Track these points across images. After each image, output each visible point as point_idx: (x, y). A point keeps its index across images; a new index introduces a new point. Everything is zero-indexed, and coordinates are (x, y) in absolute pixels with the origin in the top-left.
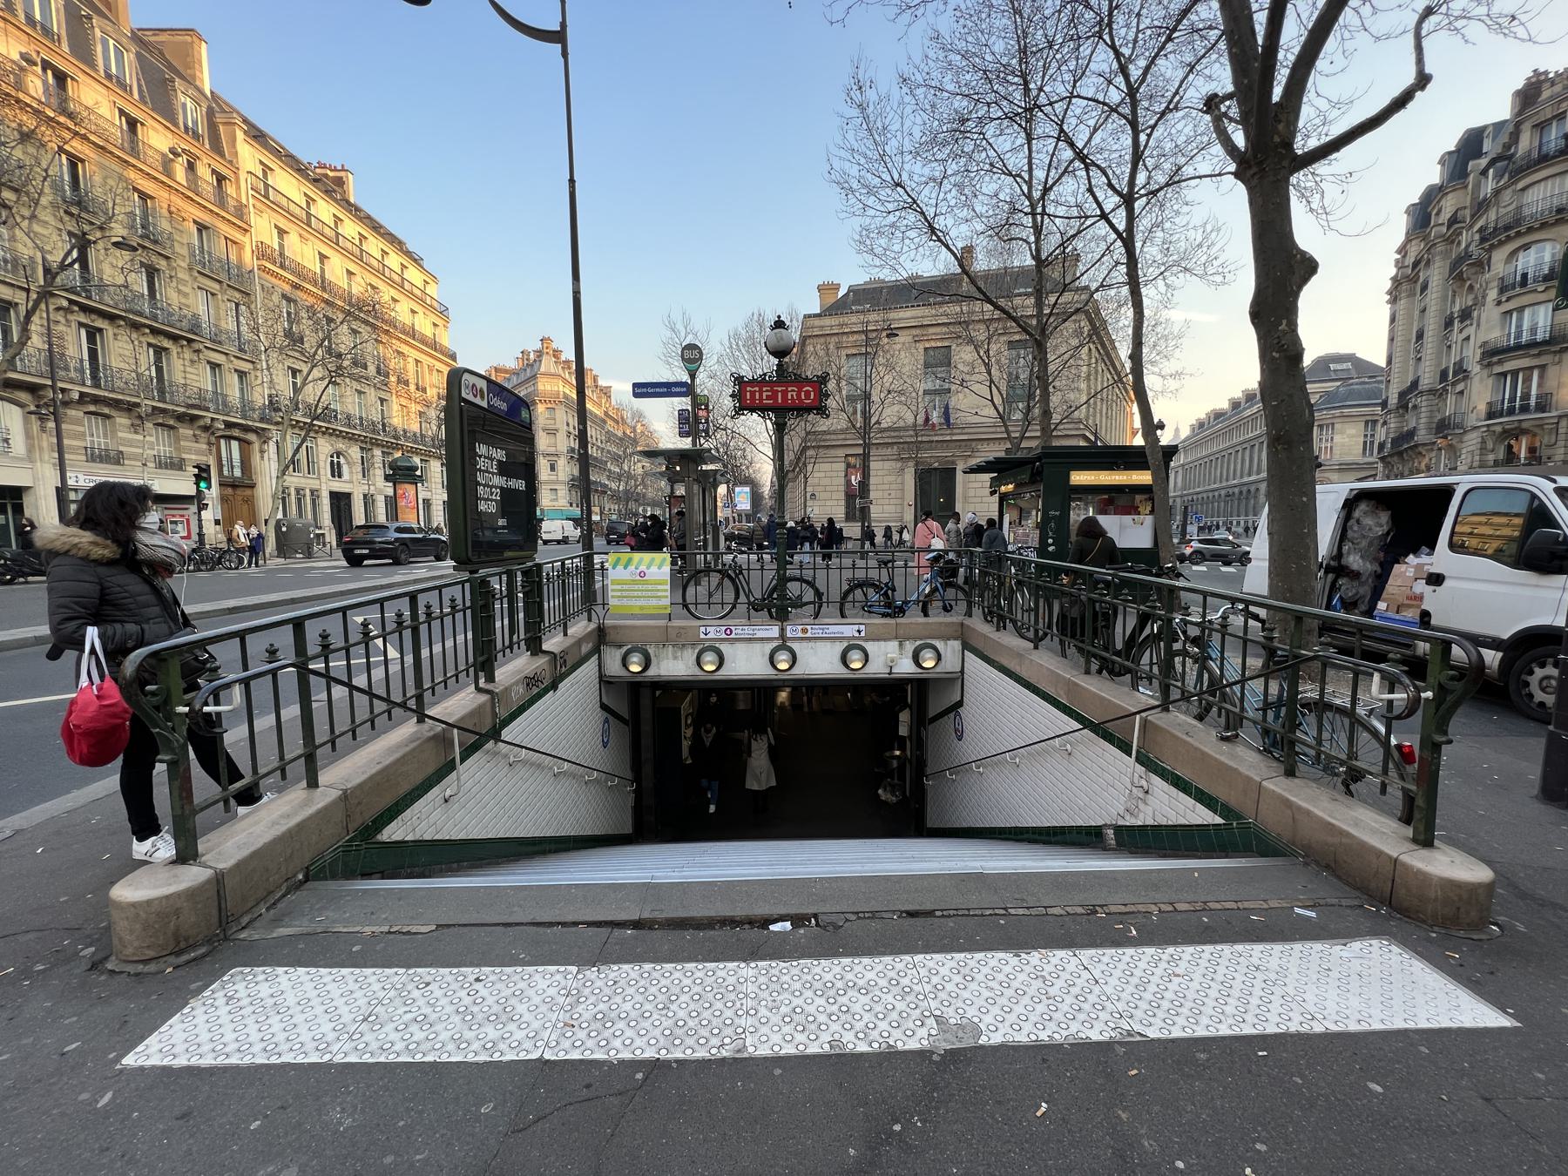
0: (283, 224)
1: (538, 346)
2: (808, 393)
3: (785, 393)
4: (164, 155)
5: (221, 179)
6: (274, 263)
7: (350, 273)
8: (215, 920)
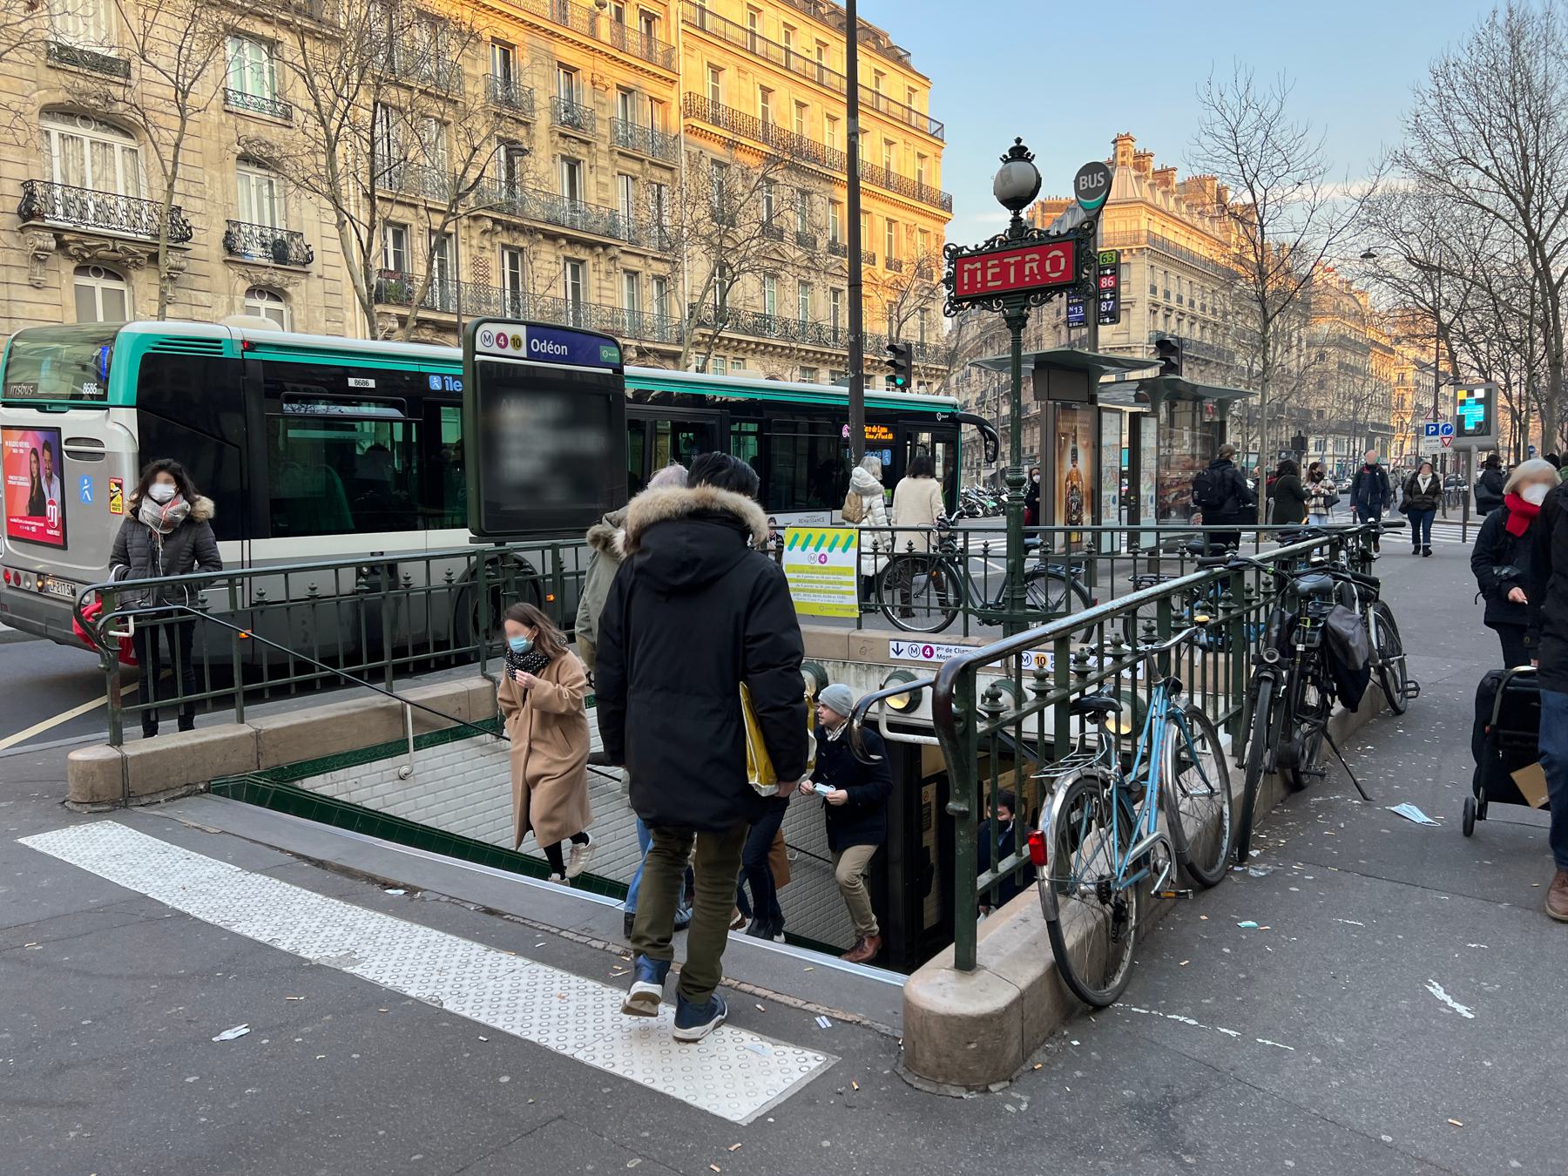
0: (718, 58)
3: (1020, 266)
4: (590, 10)
5: (649, 18)
6: (704, 118)
7: (801, 105)
8: (119, 790)
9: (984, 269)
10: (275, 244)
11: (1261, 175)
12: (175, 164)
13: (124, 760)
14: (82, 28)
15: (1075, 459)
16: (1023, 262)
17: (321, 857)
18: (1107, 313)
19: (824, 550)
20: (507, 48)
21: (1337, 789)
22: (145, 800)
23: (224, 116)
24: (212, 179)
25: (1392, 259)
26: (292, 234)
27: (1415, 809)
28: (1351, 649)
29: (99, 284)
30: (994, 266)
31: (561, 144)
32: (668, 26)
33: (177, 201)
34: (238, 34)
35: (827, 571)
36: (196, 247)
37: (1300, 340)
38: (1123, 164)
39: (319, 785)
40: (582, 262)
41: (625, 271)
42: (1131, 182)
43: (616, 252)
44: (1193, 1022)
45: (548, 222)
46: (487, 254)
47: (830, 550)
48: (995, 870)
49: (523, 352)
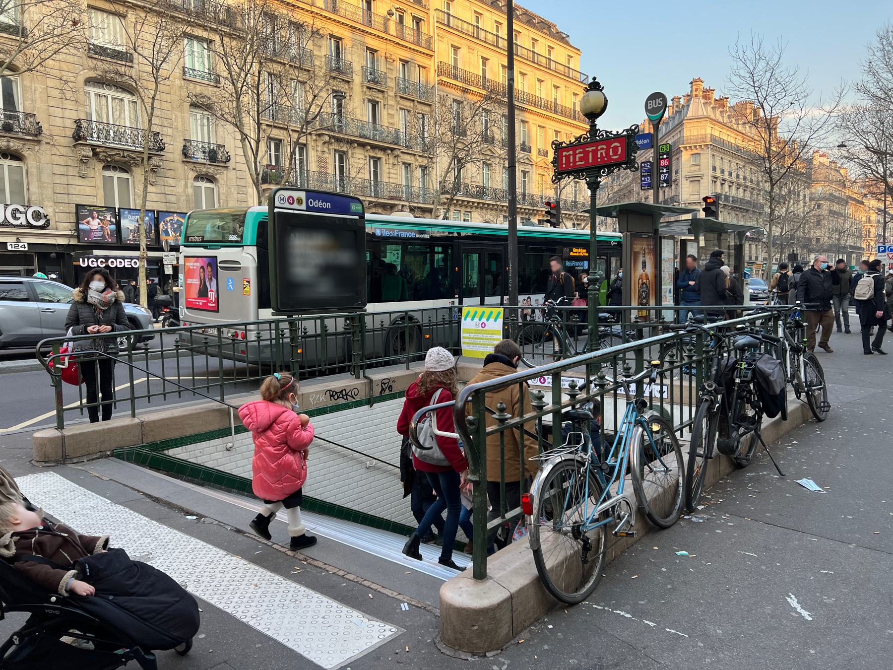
0: (457, 41)
1: (688, 90)
3: (595, 152)
4: (385, 18)
5: (418, 21)
6: (449, 76)
9: (574, 155)
10: (209, 152)
11: (769, 99)
12: (153, 108)
13: (63, 438)
14: (101, 35)
15: (644, 266)
16: (597, 150)
17: (156, 495)
18: (665, 181)
19: (484, 320)
20: (338, 40)
21: (765, 468)
22: (75, 460)
23: (183, 82)
24: (176, 117)
25: (858, 148)
26: (219, 146)
27: (811, 482)
28: (770, 381)
29: (116, 175)
30: (580, 153)
31: (368, 92)
32: (429, 24)
33: (155, 129)
34: (191, 37)
35: (487, 332)
36: (167, 154)
37: (805, 197)
38: (696, 96)
39: (179, 453)
40: (379, 159)
41: (404, 163)
42: (701, 107)
43: (398, 152)
44: (629, 616)
45: (360, 137)
46: (326, 155)
47: (488, 320)
48: (504, 517)
49: (304, 207)
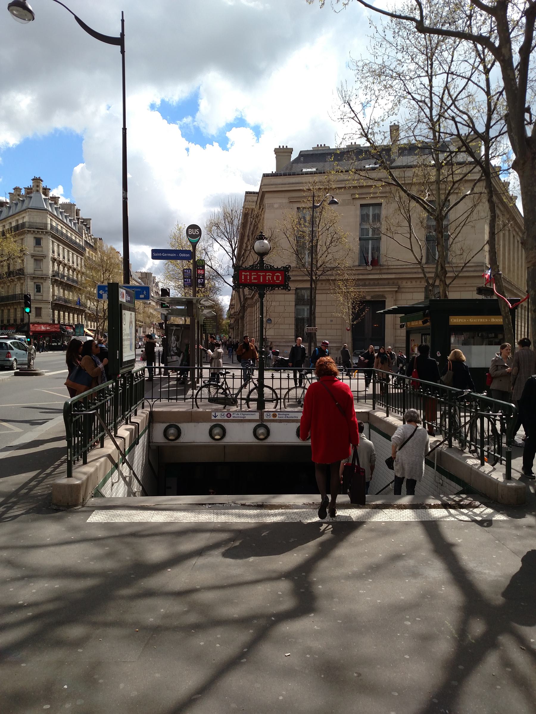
2: (278, 277)
3: (264, 277)
18: (200, 283)
30: (254, 275)
48: (501, 457)
